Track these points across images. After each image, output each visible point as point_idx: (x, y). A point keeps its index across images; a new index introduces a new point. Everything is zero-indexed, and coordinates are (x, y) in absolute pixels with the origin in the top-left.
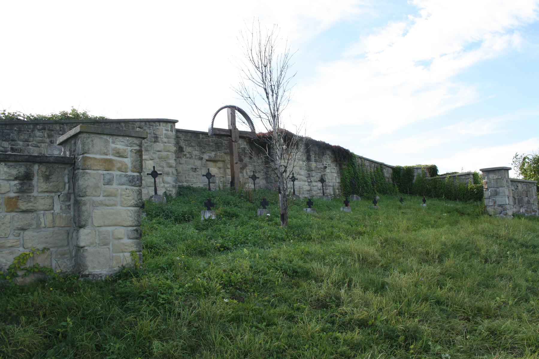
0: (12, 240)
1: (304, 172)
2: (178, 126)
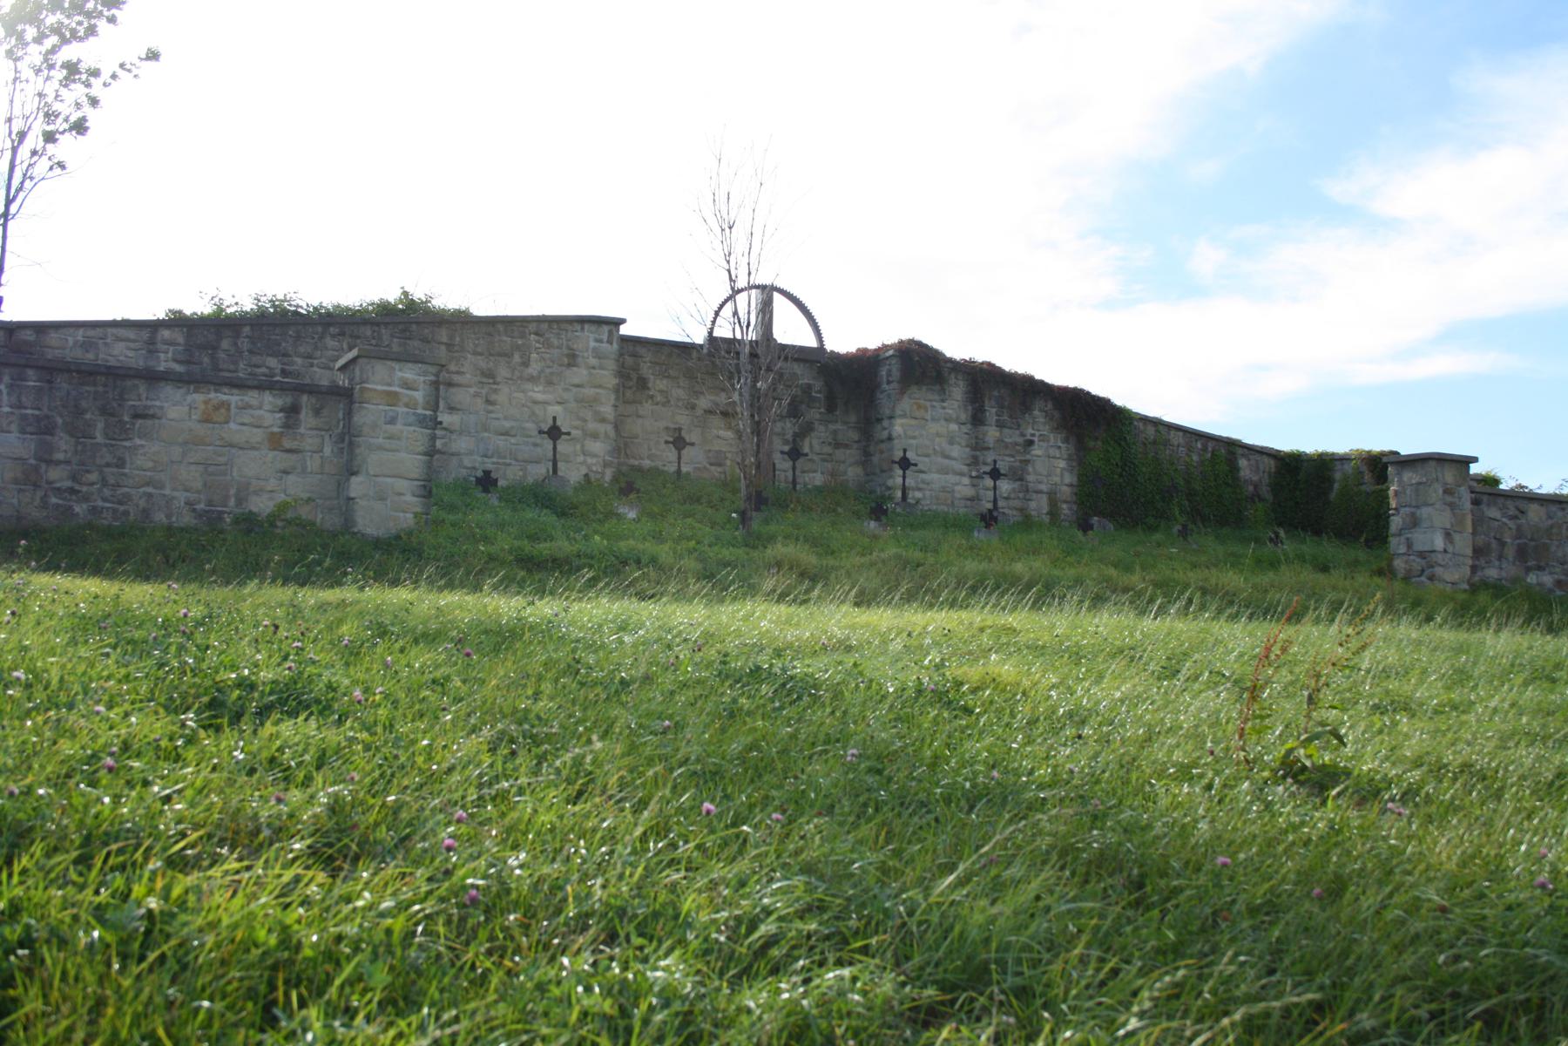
0: (272, 484)
2: (624, 330)
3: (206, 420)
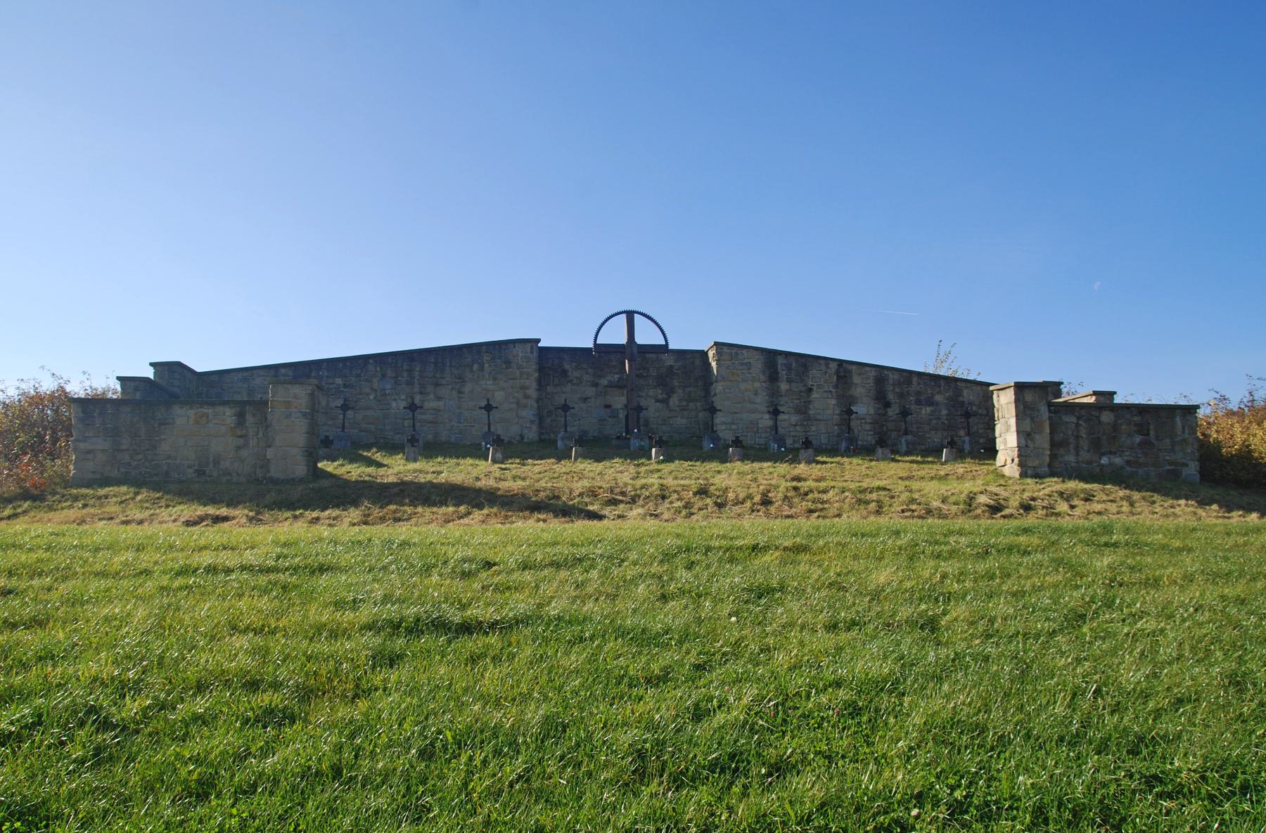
3: (197, 422)
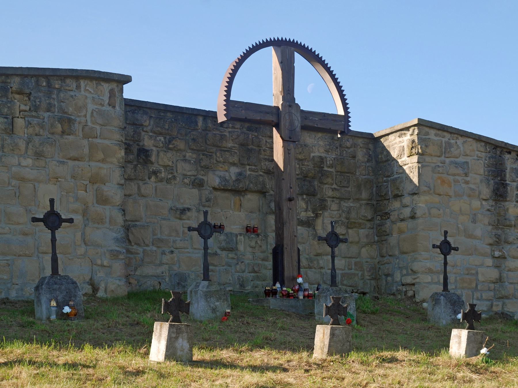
1: (482, 229)
2: (130, 92)
